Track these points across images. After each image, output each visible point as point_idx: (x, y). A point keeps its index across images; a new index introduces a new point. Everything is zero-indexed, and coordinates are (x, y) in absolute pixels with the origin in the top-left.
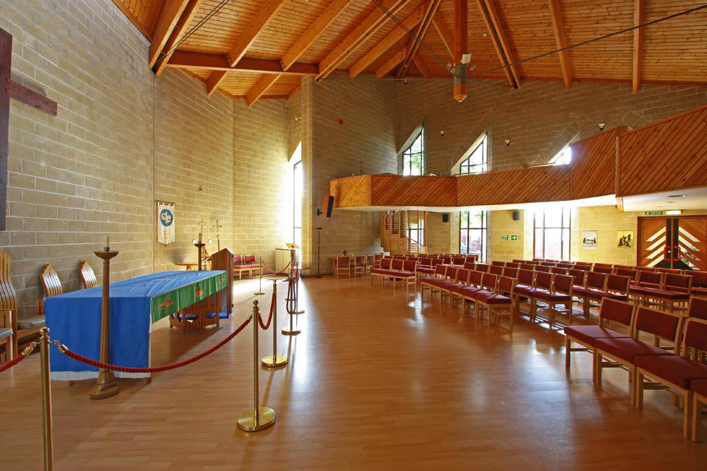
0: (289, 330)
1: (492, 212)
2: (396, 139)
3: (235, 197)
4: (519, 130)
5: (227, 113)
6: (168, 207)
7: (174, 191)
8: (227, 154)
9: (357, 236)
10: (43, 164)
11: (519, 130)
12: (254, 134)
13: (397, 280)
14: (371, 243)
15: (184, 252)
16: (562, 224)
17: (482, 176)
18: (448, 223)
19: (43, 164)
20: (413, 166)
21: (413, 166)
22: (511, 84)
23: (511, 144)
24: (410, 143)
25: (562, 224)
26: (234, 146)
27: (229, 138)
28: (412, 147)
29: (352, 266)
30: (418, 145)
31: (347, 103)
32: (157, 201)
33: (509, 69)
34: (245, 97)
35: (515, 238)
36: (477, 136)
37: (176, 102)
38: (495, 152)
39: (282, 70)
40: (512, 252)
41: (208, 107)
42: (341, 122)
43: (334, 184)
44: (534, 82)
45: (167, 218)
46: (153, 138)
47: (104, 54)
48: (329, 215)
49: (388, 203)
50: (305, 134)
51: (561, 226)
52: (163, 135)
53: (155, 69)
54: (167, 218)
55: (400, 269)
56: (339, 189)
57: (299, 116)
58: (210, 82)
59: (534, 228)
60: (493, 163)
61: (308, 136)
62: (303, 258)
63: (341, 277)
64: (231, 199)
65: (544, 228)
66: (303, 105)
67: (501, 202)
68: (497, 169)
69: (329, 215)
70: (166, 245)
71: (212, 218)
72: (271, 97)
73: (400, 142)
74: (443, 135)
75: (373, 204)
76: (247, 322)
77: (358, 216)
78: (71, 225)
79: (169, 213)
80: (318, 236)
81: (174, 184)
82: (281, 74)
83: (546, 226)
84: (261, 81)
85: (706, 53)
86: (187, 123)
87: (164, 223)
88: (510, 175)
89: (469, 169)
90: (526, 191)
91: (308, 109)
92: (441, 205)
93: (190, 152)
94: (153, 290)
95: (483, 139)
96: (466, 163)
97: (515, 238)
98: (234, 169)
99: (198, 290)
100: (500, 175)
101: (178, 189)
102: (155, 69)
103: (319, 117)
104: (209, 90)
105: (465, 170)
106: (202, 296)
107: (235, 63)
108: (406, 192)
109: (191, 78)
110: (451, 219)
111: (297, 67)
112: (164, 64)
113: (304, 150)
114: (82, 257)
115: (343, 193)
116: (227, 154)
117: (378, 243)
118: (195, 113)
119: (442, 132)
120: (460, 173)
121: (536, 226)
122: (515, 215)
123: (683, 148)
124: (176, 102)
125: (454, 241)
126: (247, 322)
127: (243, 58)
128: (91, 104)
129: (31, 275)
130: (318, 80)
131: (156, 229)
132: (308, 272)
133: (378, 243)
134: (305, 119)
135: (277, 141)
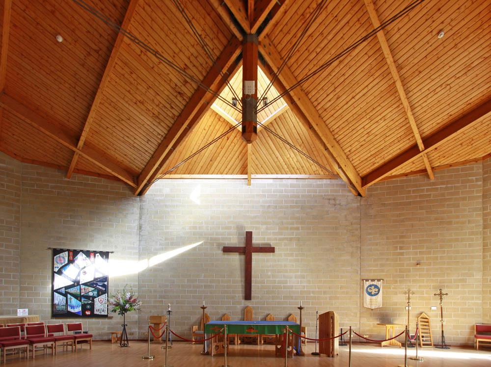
6: (375, 283)
7: (383, 271)
10: (269, 273)
15: (395, 315)
19: (269, 273)
32: (363, 280)
45: (374, 291)
52: (370, 234)
54: (374, 291)
70: (372, 310)
76: (403, 332)
78: (285, 297)
79: (376, 287)
81: (382, 265)
85: (1, 314)
87: (370, 294)
93: (402, 237)
109: (405, 178)
123: (370, 87)
126: (403, 332)
128: (298, 239)
129: (263, 317)
131: (362, 299)
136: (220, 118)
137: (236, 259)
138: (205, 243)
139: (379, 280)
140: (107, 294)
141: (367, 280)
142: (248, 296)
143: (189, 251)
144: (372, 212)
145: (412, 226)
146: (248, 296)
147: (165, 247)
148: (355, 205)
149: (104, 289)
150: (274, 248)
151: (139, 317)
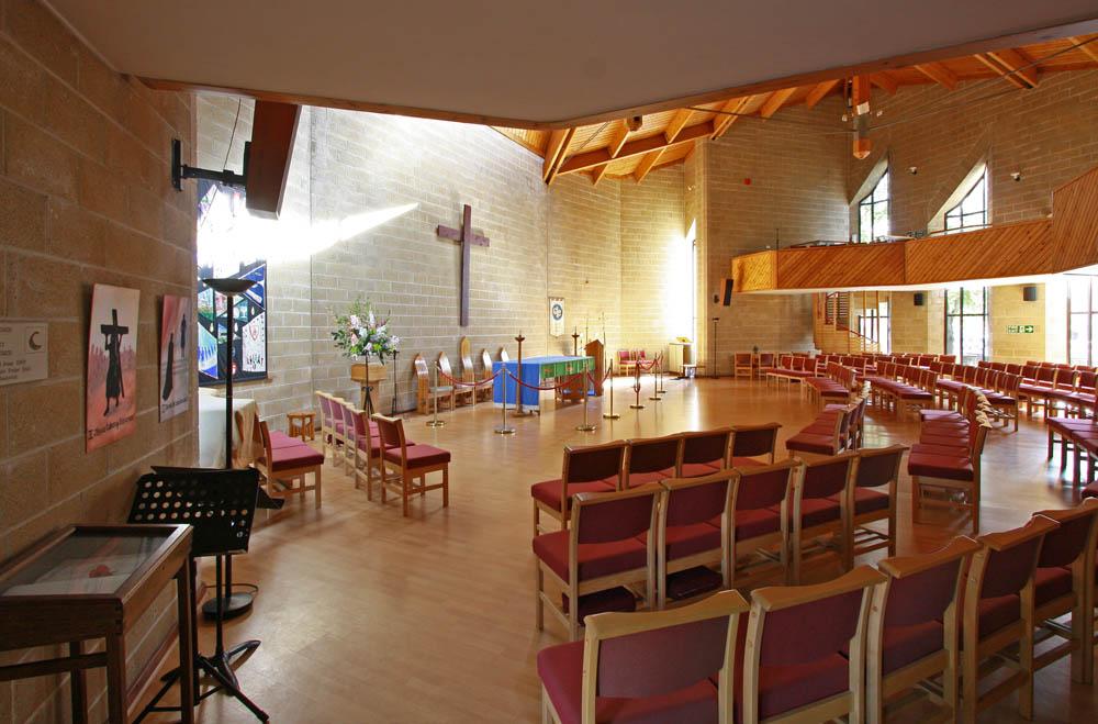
0: (635, 405)
1: (994, 288)
2: (847, 186)
3: (623, 286)
4: (1035, 154)
5: (613, 197)
7: (562, 287)
8: (615, 241)
9: (776, 329)
11: (1035, 154)
12: (643, 213)
13: (793, 381)
14: (801, 337)
16: (962, 321)
17: (977, 236)
18: (923, 308)
20: (877, 226)
21: (877, 226)
22: (1018, 85)
23: (1022, 178)
24: (870, 187)
25: (962, 321)
26: (622, 230)
27: (616, 224)
28: (875, 192)
29: (755, 366)
30: (882, 191)
31: (758, 155)
33: (980, 84)
34: (633, 174)
35: (1030, 329)
36: (968, 169)
37: (565, 203)
38: (997, 193)
39: (666, 144)
40: (1029, 353)
41: (594, 197)
42: (748, 182)
43: (736, 262)
44: (1060, 74)
46: (547, 243)
47: (513, 189)
48: (727, 302)
49: (799, 286)
50: (699, 206)
51: (1087, 310)
53: (547, 181)
55: (800, 369)
56: (742, 269)
57: (693, 183)
58: (594, 175)
59: (1069, 314)
60: (994, 211)
61: (702, 208)
62: (699, 354)
63: (741, 378)
64: (619, 289)
65: (1091, 313)
66: (696, 172)
67: (1040, 269)
68: (1001, 219)
69: (727, 302)
71: (598, 311)
72: (663, 166)
73: (853, 183)
74: (915, 173)
75: (779, 287)
76: (541, 573)
77: (777, 301)
78: (497, 321)
80: (715, 330)
81: (564, 280)
82: (665, 147)
83: (1093, 310)
84: (647, 159)
86: (575, 220)
87: (555, 316)
88: (1026, 228)
89: (962, 220)
90: (1000, 260)
91: (702, 177)
92: (914, 283)
93: (577, 247)
94: (540, 362)
95: (981, 171)
96: (957, 212)
97: (1030, 329)
98: (622, 256)
99: (569, 366)
100: (1023, 229)
101: (566, 284)
102: (547, 181)
103: (716, 182)
104: (594, 181)
105: (953, 223)
106: (571, 371)
107: (615, 155)
108: (824, 270)
110: (929, 302)
111: (687, 133)
112: (555, 174)
113: (698, 226)
114: (502, 345)
115: (746, 275)
116: (615, 241)
117: (810, 338)
118: (582, 208)
119: (913, 169)
120: (946, 229)
121: (1072, 311)
122: (1029, 293)
124: (565, 203)
125: (935, 333)
126: (541, 573)
127: (625, 145)
130: (714, 139)
132: (702, 371)
133: (810, 338)
134: (699, 187)
135: (671, 215)
136: (895, 330)
137: (450, 249)
138: (415, 213)
139: (562, 299)
140: (263, 314)
141: (553, 298)
142: (463, 322)
143: (383, 229)
144: (556, 208)
145: (583, 235)
146: (463, 322)
147: (370, 202)
148: (544, 194)
149: (259, 299)
150: (488, 239)
151: (313, 371)
